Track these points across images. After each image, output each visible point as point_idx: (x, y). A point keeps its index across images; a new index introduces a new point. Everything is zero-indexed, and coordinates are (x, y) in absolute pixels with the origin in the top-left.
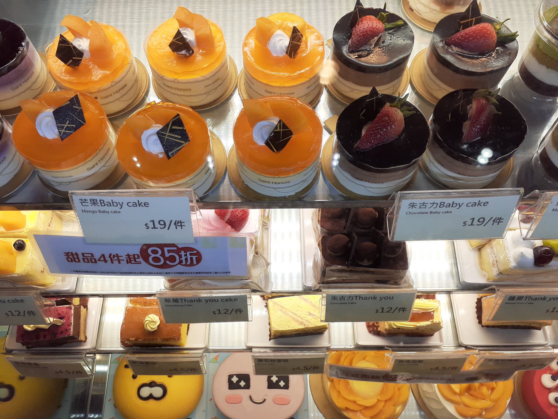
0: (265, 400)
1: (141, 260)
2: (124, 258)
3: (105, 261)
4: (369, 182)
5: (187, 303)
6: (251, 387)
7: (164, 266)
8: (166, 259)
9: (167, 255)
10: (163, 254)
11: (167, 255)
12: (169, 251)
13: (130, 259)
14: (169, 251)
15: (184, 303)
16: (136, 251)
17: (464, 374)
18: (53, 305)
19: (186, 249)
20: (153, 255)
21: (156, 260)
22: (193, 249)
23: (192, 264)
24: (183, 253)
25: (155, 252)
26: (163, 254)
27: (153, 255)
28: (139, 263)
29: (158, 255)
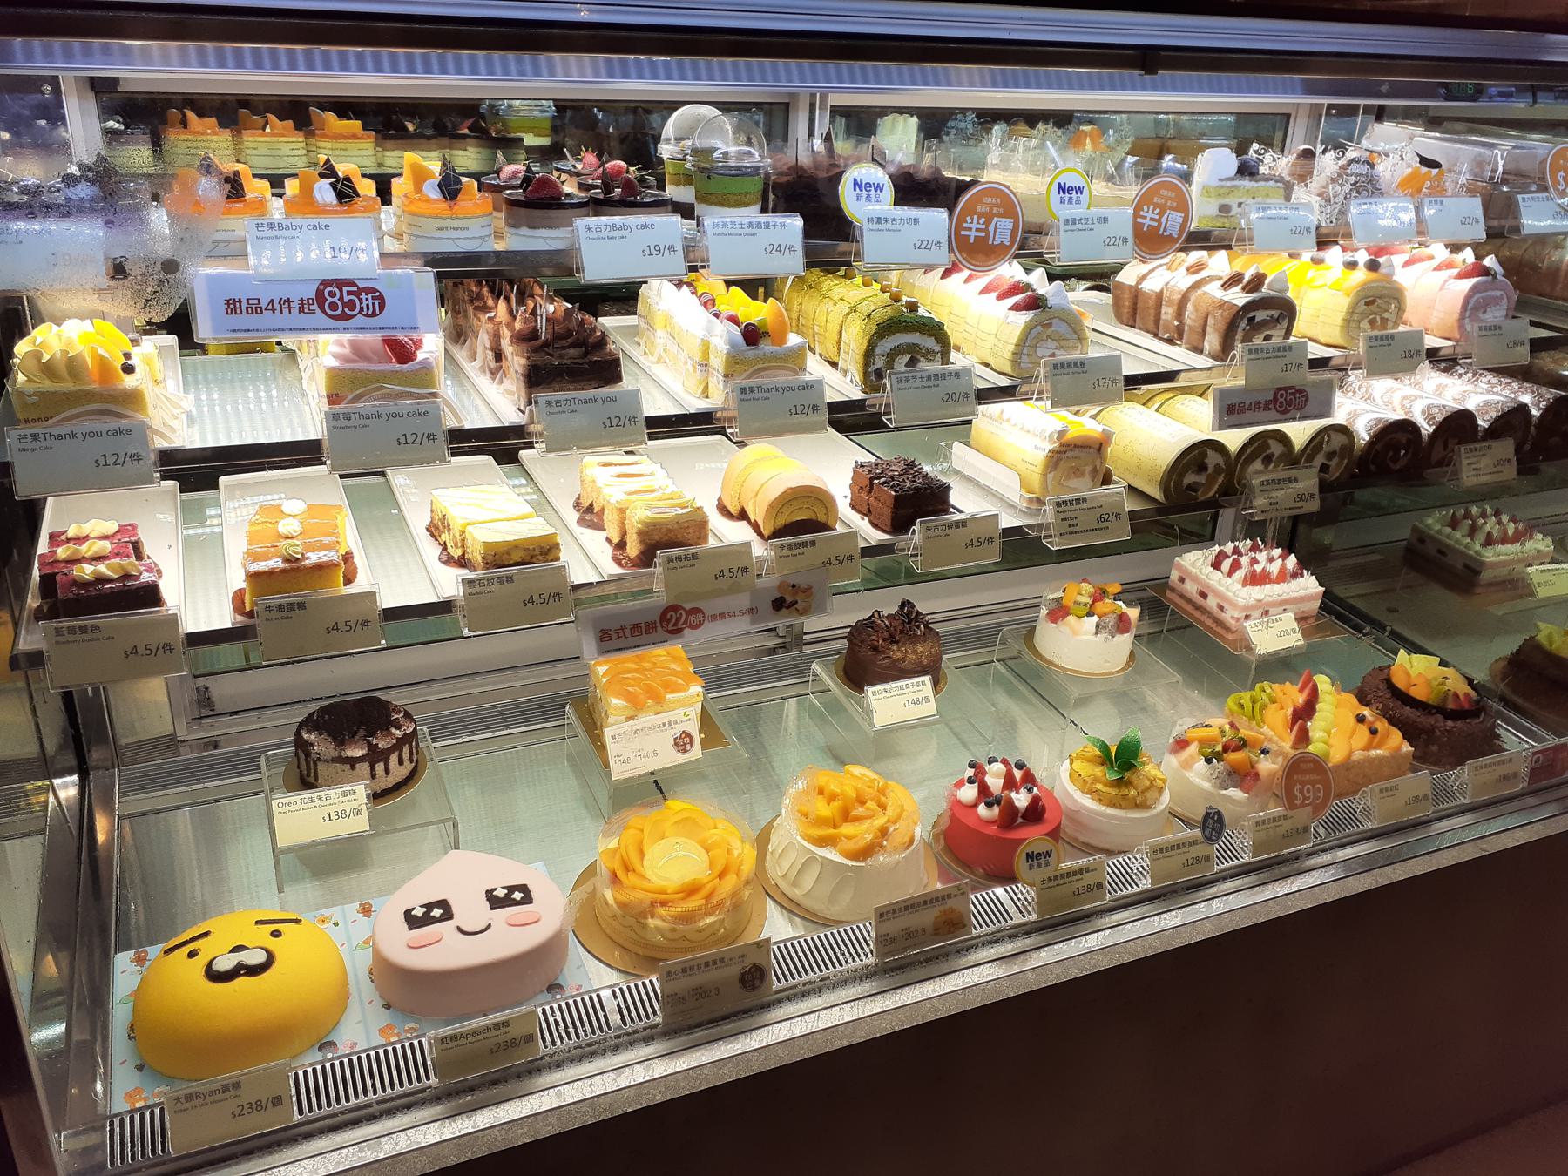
0: (257, 922)
1: (315, 307)
2: (296, 305)
3: (273, 310)
4: (550, 227)
5: (761, 395)
6: (454, 910)
7: (344, 317)
8: (345, 305)
9: (346, 299)
10: (341, 299)
11: (346, 299)
12: (349, 293)
13: (304, 306)
14: (349, 293)
15: (756, 395)
16: (310, 292)
17: (1469, 491)
18: (1196, 842)
19: (369, 290)
20: (330, 299)
21: (333, 306)
22: (375, 291)
23: (374, 315)
24: (364, 296)
25: (332, 294)
26: (341, 299)
27: (330, 299)
28: (313, 312)
29: (335, 300)
